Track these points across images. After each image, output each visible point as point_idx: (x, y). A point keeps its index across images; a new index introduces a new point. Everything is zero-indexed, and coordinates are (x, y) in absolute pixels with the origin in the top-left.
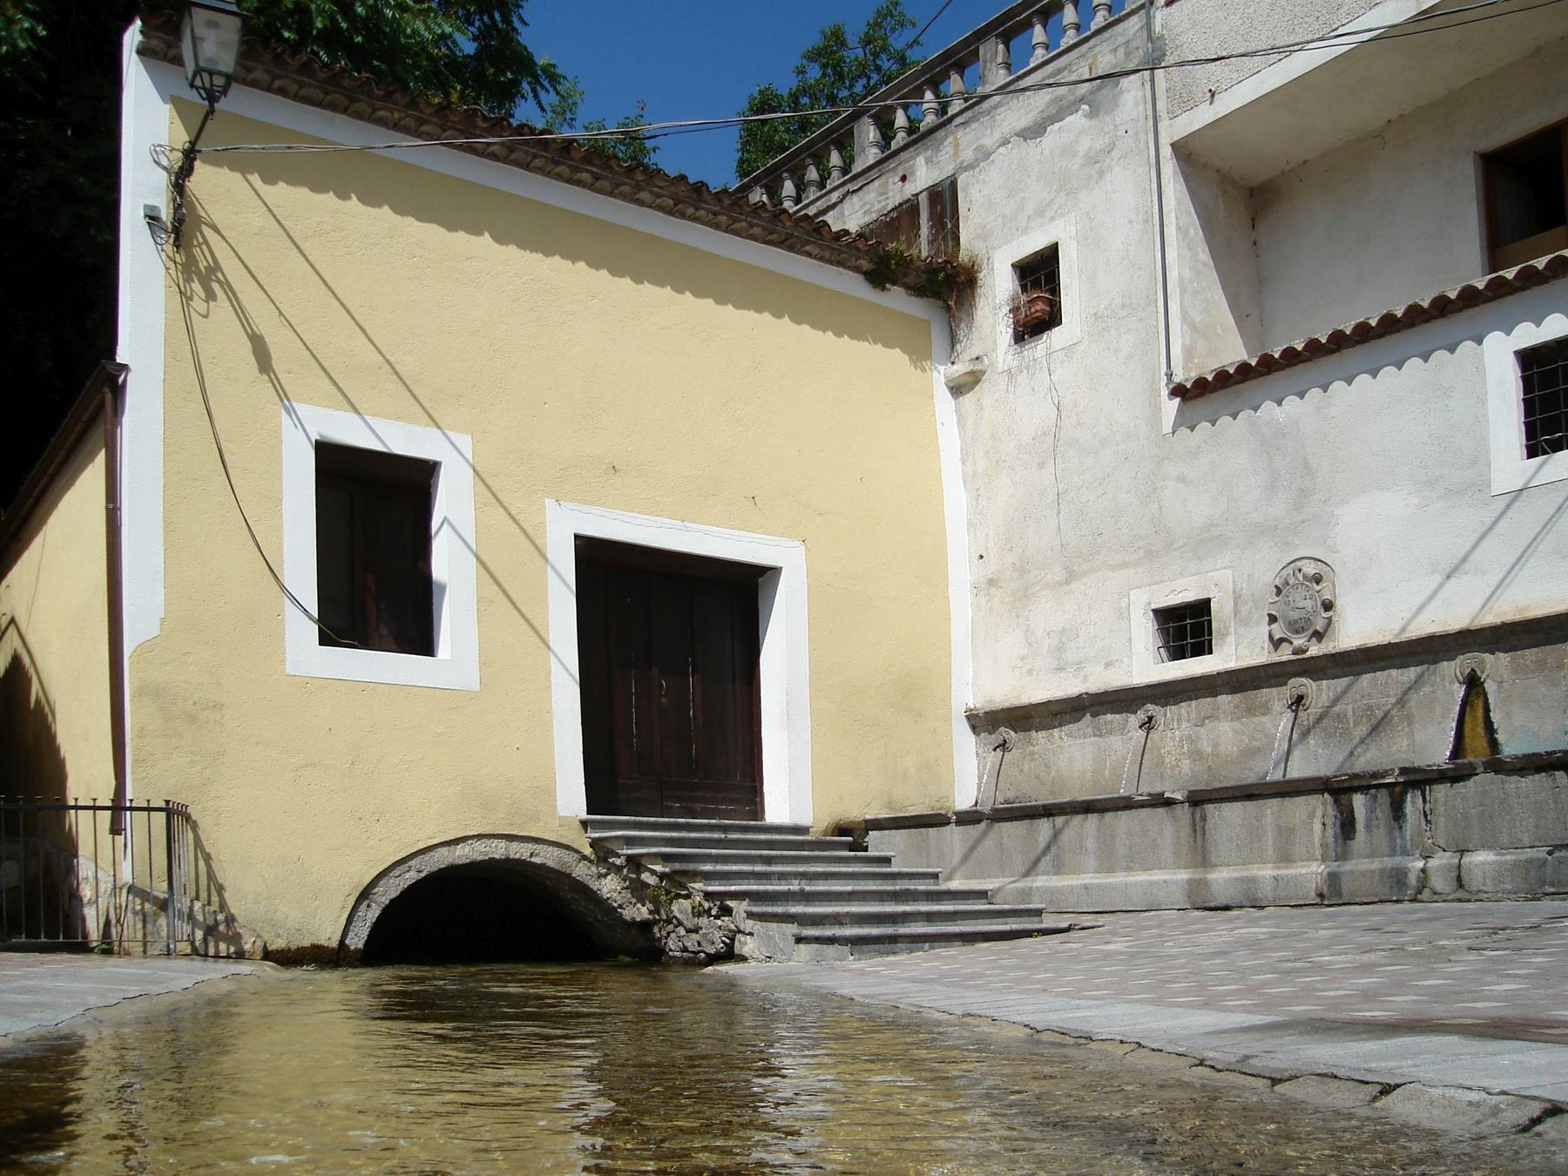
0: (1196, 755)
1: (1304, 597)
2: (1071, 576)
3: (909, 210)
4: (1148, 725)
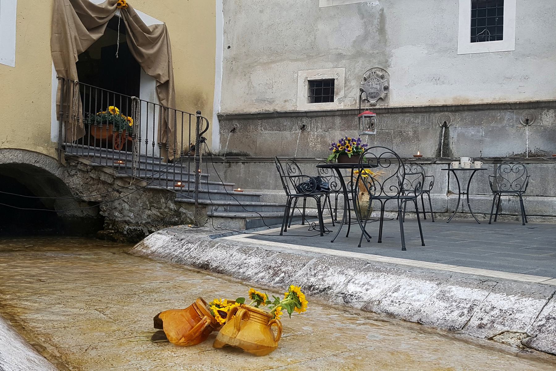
4: (303, 128)
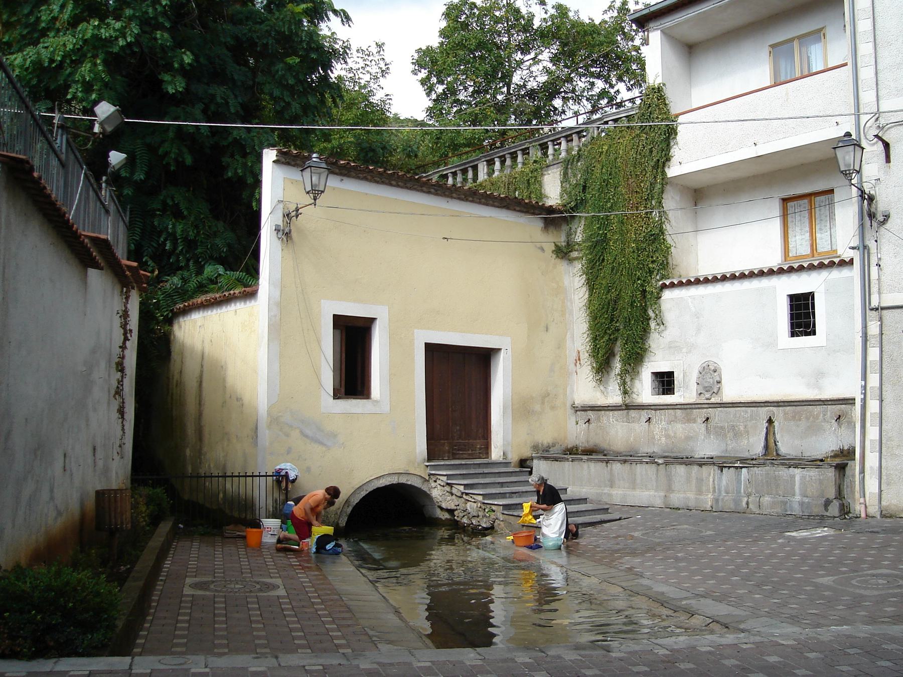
0: (668, 436)
1: (710, 378)
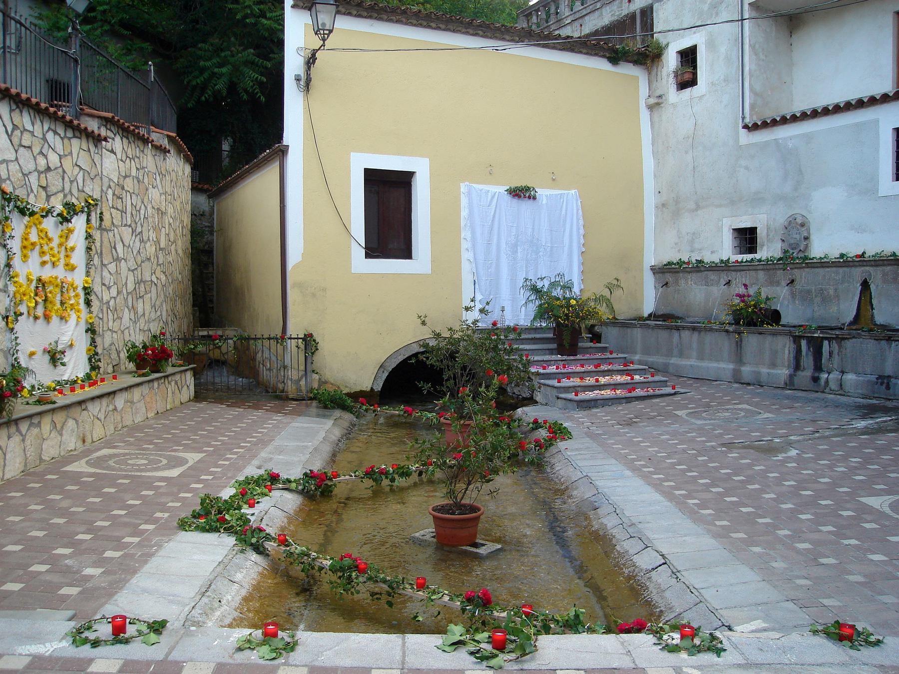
1: (797, 231)
2: (698, 207)
3: (632, 16)
